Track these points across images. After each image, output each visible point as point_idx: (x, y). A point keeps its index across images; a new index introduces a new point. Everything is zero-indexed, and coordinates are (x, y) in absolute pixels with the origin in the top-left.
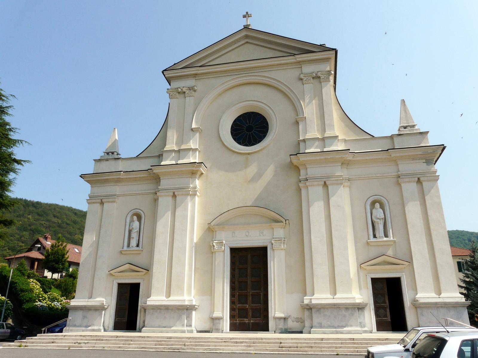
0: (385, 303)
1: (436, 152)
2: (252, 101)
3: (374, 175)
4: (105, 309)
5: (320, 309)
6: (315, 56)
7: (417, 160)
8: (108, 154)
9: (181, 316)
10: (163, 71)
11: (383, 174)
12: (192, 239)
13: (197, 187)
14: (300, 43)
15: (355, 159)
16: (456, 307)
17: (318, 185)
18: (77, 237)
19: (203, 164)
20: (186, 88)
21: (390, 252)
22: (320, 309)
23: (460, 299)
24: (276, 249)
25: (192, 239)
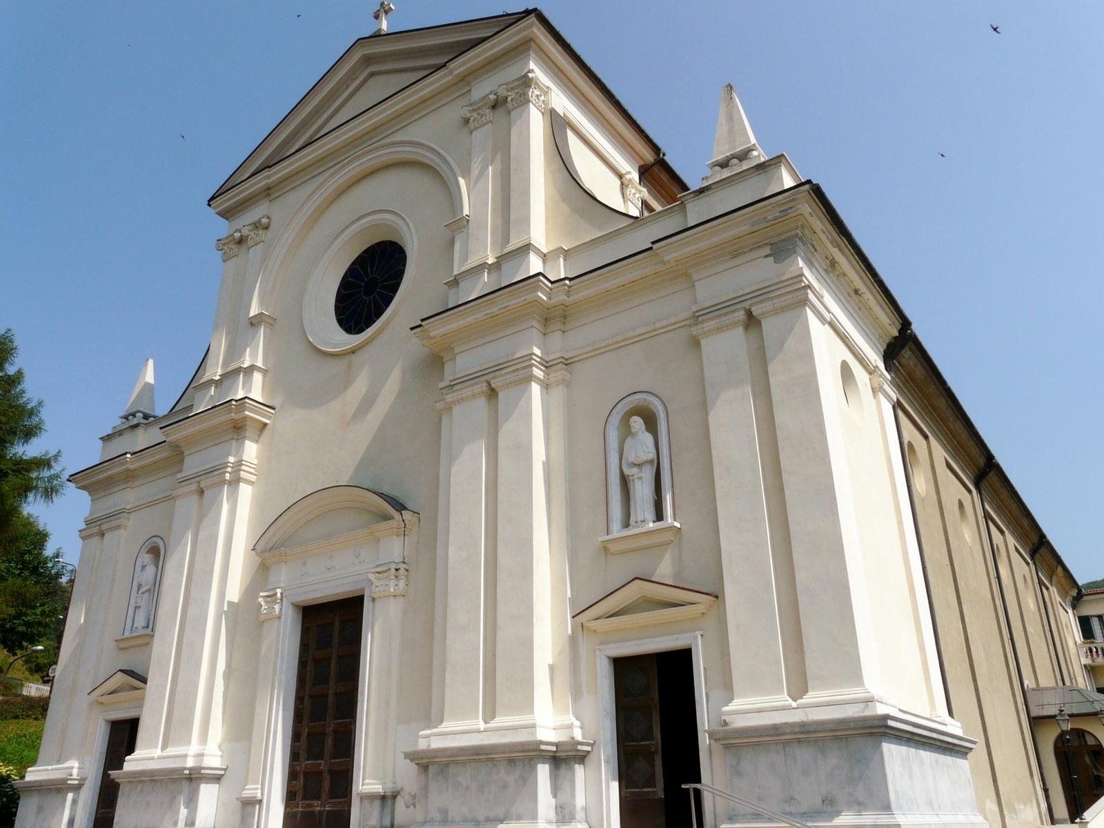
0: (651, 738)
1: (789, 211)
2: (370, 214)
3: (631, 334)
4: (77, 788)
5: (447, 765)
6: (493, 47)
7: (745, 253)
8: (126, 418)
9: (175, 797)
10: (209, 201)
11: (654, 323)
12: (222, 593)
13: (242, 460)
14: (461, 27)
15: (574, 298)
16: (846, 737)
17: (474, 396)
19: (247, 400)
20: (248, 228)
21: (665, 569)
22: (447, 765)
23: (862, 706)
24: (379, 597)
25: (222, 593)
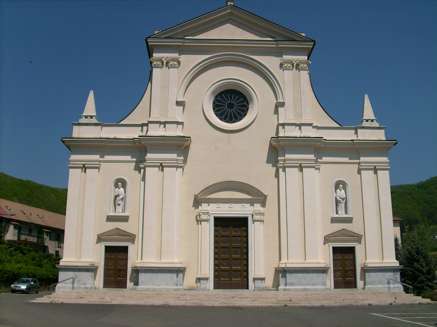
18: (339, 257)
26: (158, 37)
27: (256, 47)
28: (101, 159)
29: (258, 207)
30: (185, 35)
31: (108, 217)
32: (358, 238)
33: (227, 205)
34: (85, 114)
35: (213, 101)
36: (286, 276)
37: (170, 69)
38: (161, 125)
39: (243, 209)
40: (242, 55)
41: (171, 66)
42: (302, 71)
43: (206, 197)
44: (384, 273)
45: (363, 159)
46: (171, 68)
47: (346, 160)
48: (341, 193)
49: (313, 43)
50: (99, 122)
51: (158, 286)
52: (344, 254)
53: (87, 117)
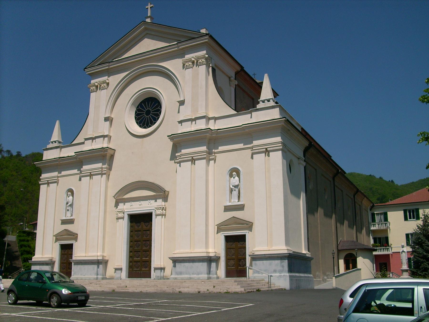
26: (93, 66)
27: (152, 57)
28: (59, 175)
29: (160, 202)
30: (113, 59)
31: (225, 207)
32: (249, 226)
33: (138, 203)
34: (52, 140)
35: (135, 111)
36: (252, 265)
37: (199, 67)
38: (193, 122)
39: (150, 205)
40: (155, 64)
41: (200, 64)
42: (201, 66)
43: (123, 197)
44: (271, 261)
45: (256, 143)
46: (200, 65)
47: (241, 146)
48: (235, 181)
49: (207, 36)
50: (63, 145)
51: (84, 276)
52: (237, 242)
53: (270, 100)
